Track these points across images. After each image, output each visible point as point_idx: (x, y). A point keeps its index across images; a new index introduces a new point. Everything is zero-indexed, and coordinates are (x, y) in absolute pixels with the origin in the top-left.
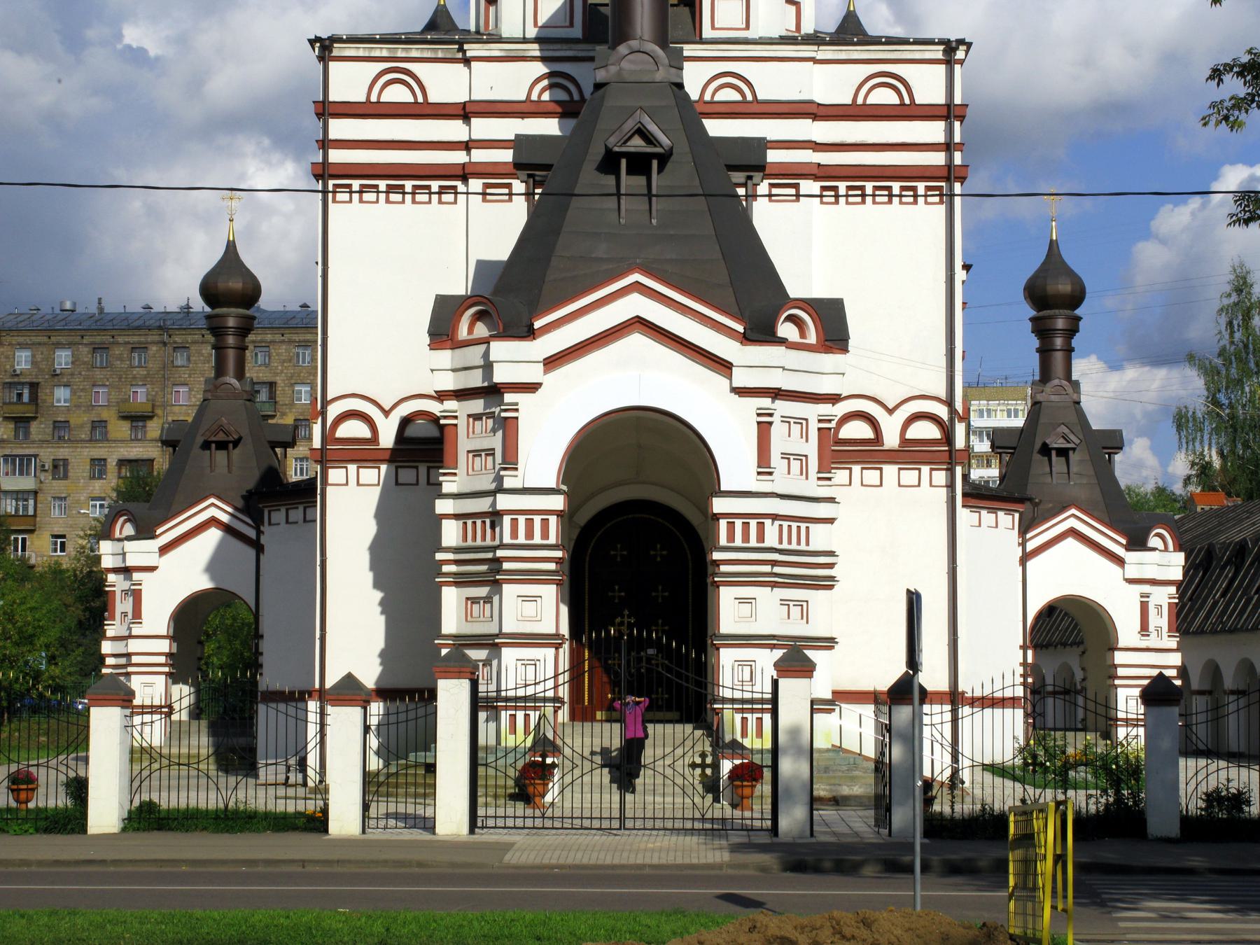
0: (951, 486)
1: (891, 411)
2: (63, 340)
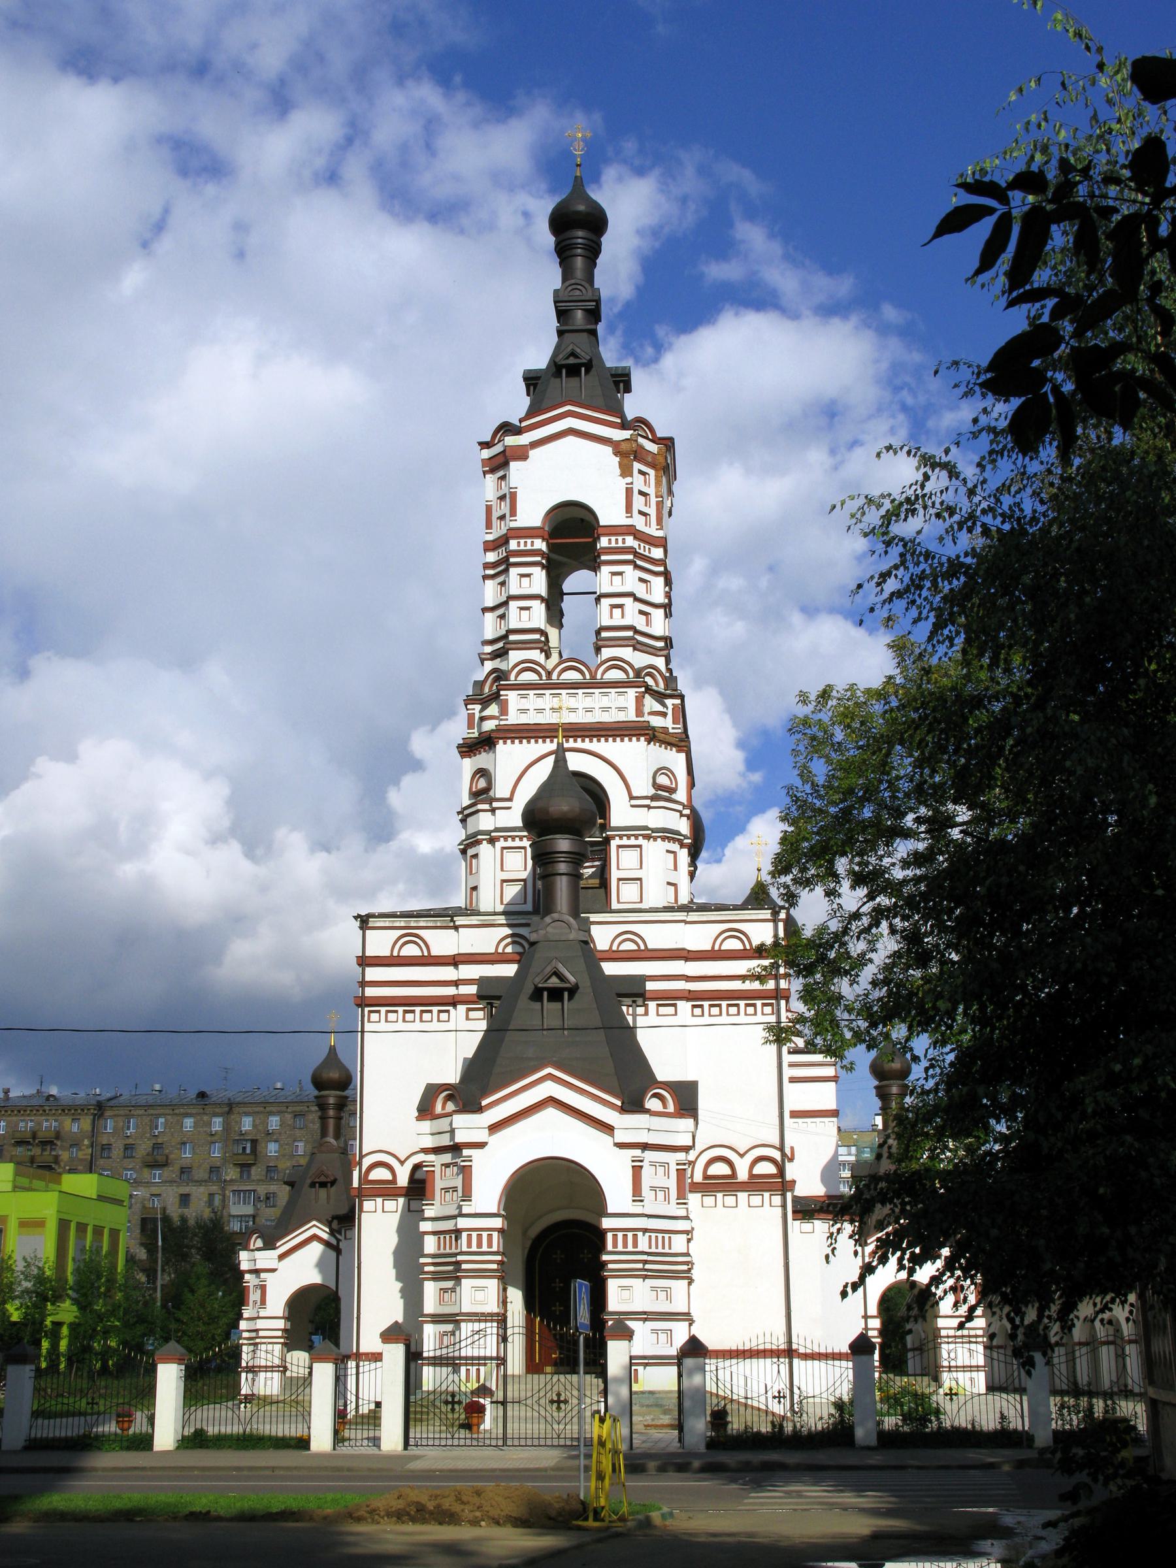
0: (784, 1206)
1: (742, 1156)
2: (274, 1109)
